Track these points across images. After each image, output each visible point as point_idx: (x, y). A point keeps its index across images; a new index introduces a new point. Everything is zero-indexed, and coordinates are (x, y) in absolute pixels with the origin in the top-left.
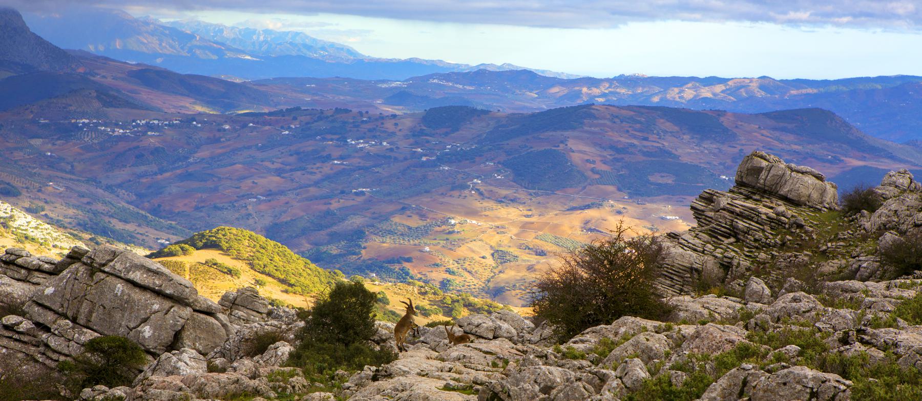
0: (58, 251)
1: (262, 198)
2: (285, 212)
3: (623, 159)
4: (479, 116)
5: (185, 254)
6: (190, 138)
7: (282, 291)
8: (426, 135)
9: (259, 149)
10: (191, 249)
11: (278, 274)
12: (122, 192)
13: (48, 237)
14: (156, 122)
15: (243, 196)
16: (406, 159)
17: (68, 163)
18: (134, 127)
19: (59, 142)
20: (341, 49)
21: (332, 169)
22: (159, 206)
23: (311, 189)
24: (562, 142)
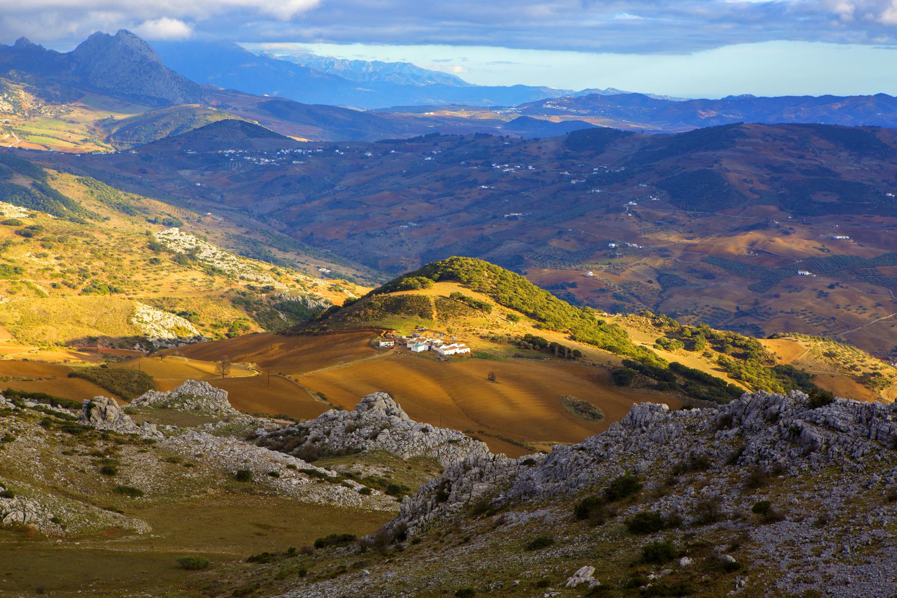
0: (245, 283)
1: (414, 225)
2: (438, 238)
3: (780, 177)
4: (623, 137)
5: (423, 287)
6: (334, 166)
7: (534, 327)
8: (572, 158)
9: (404, 175)
10: (431, 282)
11: (525, 308)
12: (273, 221)
13: (234, 268)
14: (300, 151)
15: (394, 223)
16: (553, 183)
17: (218, 193)
18: (279, 156)
19: (208, 173)
20: (448, 77)
21: (480, 194)
22: (312, 234)
23: (462, 214)
24: (715, 162)
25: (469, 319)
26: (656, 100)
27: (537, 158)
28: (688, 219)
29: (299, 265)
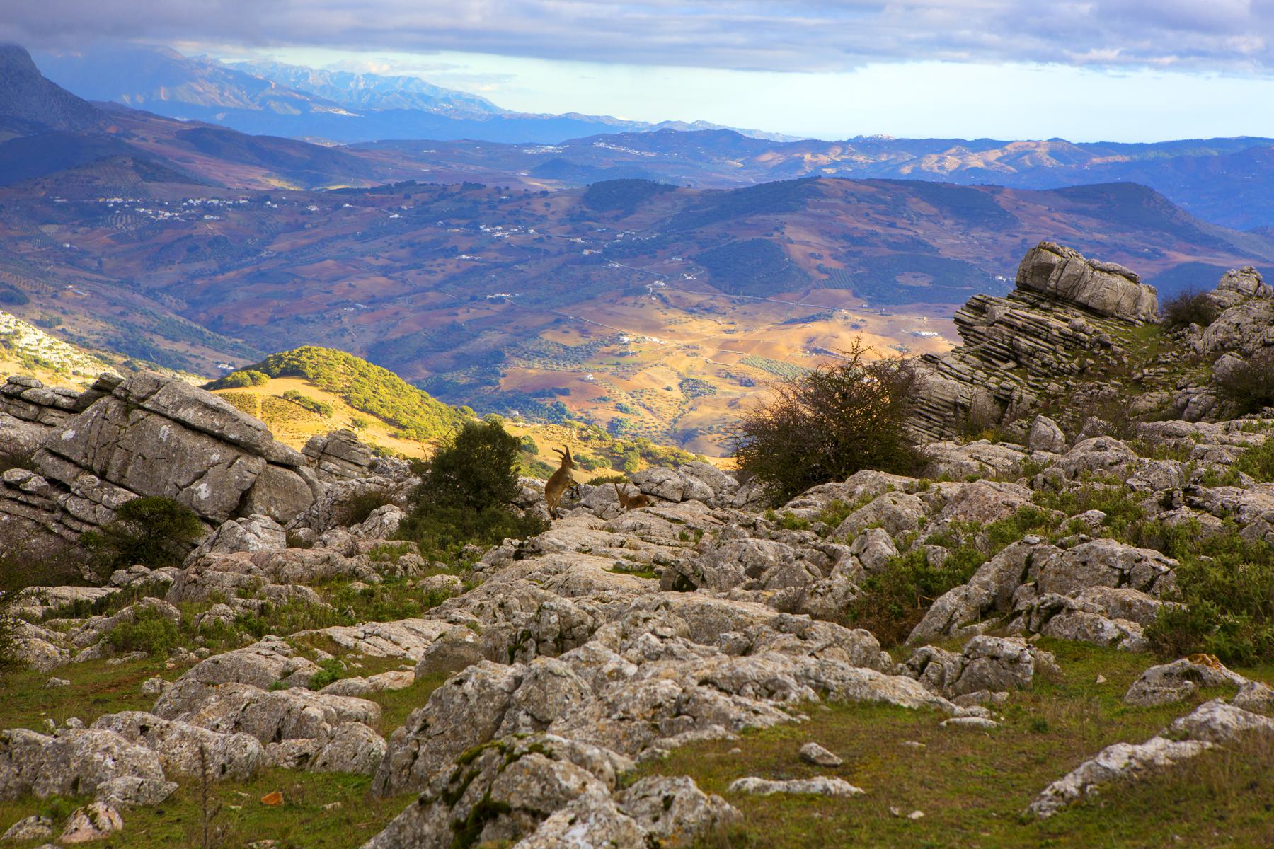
0: (80, 380)
4: (661, 193)
5: (255, 385)
7: (390, 436)
9: (357, 239)
10: (264, 377)
11: (383, 412)
12: (168, 298)
13: (66, 360)
14: (215, 201)
15: (336, 304)
17: (94, 259)
18: (185, 208)
21: (458, 267)
22: (220, 318)
23: (430, 294)
24: (776, 229)
25: (300, 424)
26: (753, 140)
27: (542, 218)
28: (731, 305)
29: (191, 359)
